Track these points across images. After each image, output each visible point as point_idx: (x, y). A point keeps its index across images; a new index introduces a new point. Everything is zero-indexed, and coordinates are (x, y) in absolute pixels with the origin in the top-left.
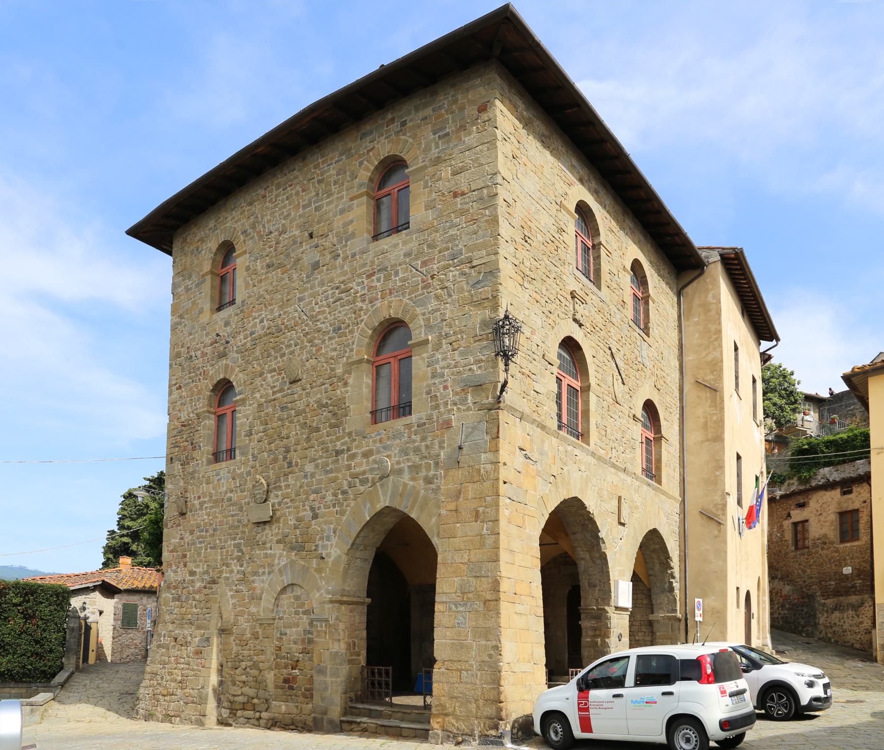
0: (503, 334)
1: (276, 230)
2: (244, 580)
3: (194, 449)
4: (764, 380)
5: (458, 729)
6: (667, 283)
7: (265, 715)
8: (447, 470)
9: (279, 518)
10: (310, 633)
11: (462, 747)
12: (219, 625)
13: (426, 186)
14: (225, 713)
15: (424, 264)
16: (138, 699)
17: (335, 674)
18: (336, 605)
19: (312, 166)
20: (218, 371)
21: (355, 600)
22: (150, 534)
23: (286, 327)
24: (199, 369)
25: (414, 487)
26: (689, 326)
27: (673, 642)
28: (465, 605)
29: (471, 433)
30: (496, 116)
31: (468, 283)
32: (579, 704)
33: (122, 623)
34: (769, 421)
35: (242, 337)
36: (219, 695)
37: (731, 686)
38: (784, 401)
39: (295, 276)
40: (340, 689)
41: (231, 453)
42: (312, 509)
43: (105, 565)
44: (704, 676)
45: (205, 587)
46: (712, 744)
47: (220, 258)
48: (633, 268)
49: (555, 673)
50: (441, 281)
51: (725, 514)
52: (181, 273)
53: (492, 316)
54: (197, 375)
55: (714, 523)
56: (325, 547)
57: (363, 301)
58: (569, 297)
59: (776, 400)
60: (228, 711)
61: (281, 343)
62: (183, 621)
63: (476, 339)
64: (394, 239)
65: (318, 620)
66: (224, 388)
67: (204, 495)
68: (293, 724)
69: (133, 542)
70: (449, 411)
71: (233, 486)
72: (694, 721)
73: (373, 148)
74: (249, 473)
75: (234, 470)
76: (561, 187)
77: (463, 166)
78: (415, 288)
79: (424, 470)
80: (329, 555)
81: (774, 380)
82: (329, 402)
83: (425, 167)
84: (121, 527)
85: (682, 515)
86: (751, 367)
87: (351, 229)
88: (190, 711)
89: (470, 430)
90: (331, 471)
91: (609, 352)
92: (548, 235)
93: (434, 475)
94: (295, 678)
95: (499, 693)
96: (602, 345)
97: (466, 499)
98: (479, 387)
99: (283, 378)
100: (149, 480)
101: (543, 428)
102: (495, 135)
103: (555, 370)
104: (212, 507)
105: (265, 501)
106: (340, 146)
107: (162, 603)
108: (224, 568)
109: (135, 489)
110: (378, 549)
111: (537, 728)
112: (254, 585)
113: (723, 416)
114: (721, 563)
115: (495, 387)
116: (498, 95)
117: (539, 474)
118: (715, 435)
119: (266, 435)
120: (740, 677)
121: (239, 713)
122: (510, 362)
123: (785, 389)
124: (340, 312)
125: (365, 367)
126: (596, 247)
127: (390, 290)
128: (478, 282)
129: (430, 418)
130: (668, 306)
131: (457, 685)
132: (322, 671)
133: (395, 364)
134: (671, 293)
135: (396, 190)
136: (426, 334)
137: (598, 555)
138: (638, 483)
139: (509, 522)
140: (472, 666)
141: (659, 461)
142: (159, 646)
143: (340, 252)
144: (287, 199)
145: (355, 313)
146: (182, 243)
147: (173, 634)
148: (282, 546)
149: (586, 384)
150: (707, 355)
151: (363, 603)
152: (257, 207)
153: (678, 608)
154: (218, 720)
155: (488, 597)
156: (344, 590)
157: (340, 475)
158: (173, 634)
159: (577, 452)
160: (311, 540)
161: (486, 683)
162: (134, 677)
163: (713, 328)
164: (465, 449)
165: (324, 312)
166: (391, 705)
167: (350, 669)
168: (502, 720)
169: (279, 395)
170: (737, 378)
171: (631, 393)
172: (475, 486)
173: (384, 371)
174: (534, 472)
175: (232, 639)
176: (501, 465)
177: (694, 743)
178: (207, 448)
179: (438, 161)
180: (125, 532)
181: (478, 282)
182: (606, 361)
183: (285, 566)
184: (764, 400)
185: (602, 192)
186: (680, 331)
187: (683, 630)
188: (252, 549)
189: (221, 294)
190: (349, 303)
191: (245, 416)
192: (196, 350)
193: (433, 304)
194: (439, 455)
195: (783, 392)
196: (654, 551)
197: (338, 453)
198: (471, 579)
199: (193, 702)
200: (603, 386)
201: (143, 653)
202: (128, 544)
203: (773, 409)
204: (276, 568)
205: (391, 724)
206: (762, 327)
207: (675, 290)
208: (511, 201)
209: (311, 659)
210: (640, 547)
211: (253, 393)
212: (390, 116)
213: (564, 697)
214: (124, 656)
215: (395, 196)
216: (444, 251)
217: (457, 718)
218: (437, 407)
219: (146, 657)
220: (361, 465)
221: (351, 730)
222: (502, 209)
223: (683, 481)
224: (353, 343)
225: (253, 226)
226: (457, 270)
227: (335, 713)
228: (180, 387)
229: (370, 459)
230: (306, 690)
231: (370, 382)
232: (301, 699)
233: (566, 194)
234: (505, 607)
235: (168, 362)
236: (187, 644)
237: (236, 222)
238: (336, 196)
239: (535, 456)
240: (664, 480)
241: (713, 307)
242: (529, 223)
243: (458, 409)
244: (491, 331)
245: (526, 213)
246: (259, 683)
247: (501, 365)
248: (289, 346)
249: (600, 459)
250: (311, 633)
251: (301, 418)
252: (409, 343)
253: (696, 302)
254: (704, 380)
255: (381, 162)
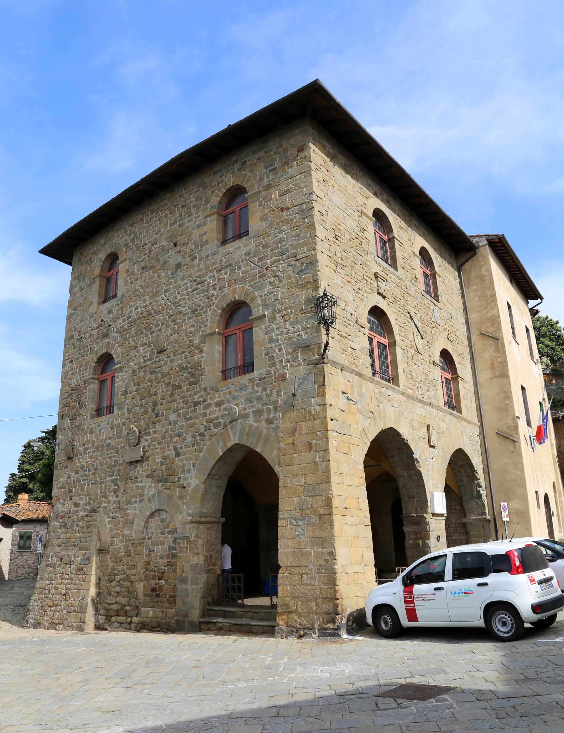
0: (323, 307)
1: (149, 243)
2: (119, 508)
3: (81, 407)
4: (535, 329)
5: (300, 624)
6: (449, 263)
7: (135, 620)
8: (284, 412)
9: (149, 457)
10: (174, 549)
11: (304, 640)
12: (98, 546)
13: (260, 205)
14: (102, 619)
15: (260, 260)
16: (28, 610)
17: (195, 582)
18: (196, 525)
19: (178, 196)
20: (101, 348)
21: (211, 520)
22: (43, 475)
23: (155, 312)
24: (87, 346)
25: (258, 427)
26: (469, 292)
27: (486, 540)
28: (304, 519)
29: (302, 383)
30: (310, 154)
31: (294, 272)
32: (405, 597)
33: (19, 547)
34: (545, 359)
35: (121, 321)
36: (96, 604)
37: (538, 575)
38: (554, 344)
39: (163, 274)
40: (199, 595)
41: (110, 409)
42: (175, 449)
43: (7, 501)
44: (513, 567)
45: (87, 516)
46: (527, 625)
47: (107, 265)
48: (421, 253)
49: (384, 573)
50: (274, 271)
51: (517, 433)
52: (77, 278)
53: (314, 294)
54: (85, 351)
55: (509, 441)
56: (186, 479)
57: (215, 289)
58: (373, 277)
59: (547, 342)
60: (104, 617)
61: (151, 324)
62: (67, 545)
63: (303, 312)
64: (237, 243)
65: (183, 538)
66: (106, 360)
67: (88, 443)
68: (159, 626)
69: (30, 482)
70: (284, 367)
71: (111, 434)
72: (508, 607)
73: (222, 181)
74: (124, 424)
75: (112, 422)
76: (360, 199)
77: (287, 190)
78: (254, 277)
79: (265, 414)
80: (189, 485)
81: (544, 328)
82: (188, 366)
83: (260, 192)
84: (21, 470)
85: (482, 437)
86: (523, 319)
87: (205, 238)
88: (72, 619)
89: (302, 381)
90: (190, 418)
91: (408, 316)
92: (354, 233)
93: (274, 417)
94: (161, 587)
95: (335, 592)
96: (402, 311)
97: (301, 435)
98: (306, 348)
99: (153, 349)
100: (45, 432)
101: (360, 375)
102: (310, 167)
103: (367, 331)
104: (94, 452)
105: (137, 445)
106: (198, 181)
107: (51, 531)
108: (103, 499)
109: (34, 441)
110: (230, 477)
111: (369, 620)
112: (127, 512)
113: (505, 358)
114: (519, 473)
115: (320, 347)
116: (311, 140)
117: (359, 411)
118: (501, 372)
119: (138, 394)
120: (546, 567)
121: (113, 619)
122: (330, 328)
123: (554, 334)
124: (196, 298)
125: (216, 337)
126: (391, 240)
127: (235, 280)
128: (301, 271)
129: (269, 373)
130: (451, 279)
131: (298, 587)
132: (183, 581)
133: (240, 335)
134: (452, 270)
135: (239, 209)
136: (263, 311)
137: (414, 473)
138: (442, 414)
139: (337, 451)
140: (312, 570)
141: (458, 395)
142: (47, 566)
143: (197, 255)
144: (159, 220)
145: (208, 298)
146: (80, 255)
147: (59, 555)
148: (150, 479)
149: (392, 341)
150: (486, 313)
151: (218, 522)
152: (137, 227)
153: (487, 511)
154: (95, 625)
155: (323, 512)
156: (202, 512)
157: (198, 421)
158: (59, 555)
159: (389, 392)
160: (174, 473)
161: (324, 584)
162: (27, 592)
163: (489, 293)
164: (298, 395)
165: (184, 299)
166: (243, 606)
167: (207, 577)
168: (338, 614)
169: (149, 363)
170: (513, 329)
171: (429, 345)
172: (308, 424)
173: (232, 340)
174: (354, 412)
175: (109, 557)
176: (328, 406)
177: (510, 626)
178: (91, 406)
179: (269, 187)
180: (24, 474)
181: (301, 271)
182: (407, 323)
183: (153, 495)
184: (538, 344)
185: (392, 202)
186: (463, 297)
187: (492, 529)
188: (126, 483)
189: (107, 290)
190: (203, 291)
191: (121, 380)
192: (85, 333)
193: (268, 288)
194: (277, 401)
195: (553, 337)
196: (461, 466)
197: (196, 404)
198: (308, 498)
199: (74, 611)
200: (406, 341)
201: (35, 571)
202: (26, 483)
203: (546, 350)
204: (146, 498)
205: (243, 623)
206: (528, 291)
207: (455, 267)
208: (324, 212)
209: (174, 571)
210: (449, 464)
211: (128, 362)
212: (234, 159)
213: (392, 592)
214: (19, 575)
215: (238, 213)
216: (275, 250)
217: (299, 615)
218: (274, 364)
219: (36, 574)
220: (215, 413)
221: (209, 630)
222: (317, 218)
223: (479, 410)
224: (207, 321)
225: (133, 241)
226: (285, 263)
227: (195, 615)
228: (72, 361)
229: (222, 407)
230: (170, 597)
231: (220, 348)
232: (166, 605)
233: (365, 204)
234: (337, 520)
235: (63, 343)
236: (70, 563)
237: (121, 239)
238: (194, 215)
239: (355, 398)
240: (463, 410)
241: (486, 277)
242: (338, 226)
243: (291, 365)
244: (313, 305)
245: (336, 220)
246: (131, 593)
247: (323, 331)
248: (157, 325)
249: (409, 397)
250: (175, 549)
251: (166, 379)
252: (250, 318)
253: (473, 275)
254: (486, 332)
255: (228, 190)
